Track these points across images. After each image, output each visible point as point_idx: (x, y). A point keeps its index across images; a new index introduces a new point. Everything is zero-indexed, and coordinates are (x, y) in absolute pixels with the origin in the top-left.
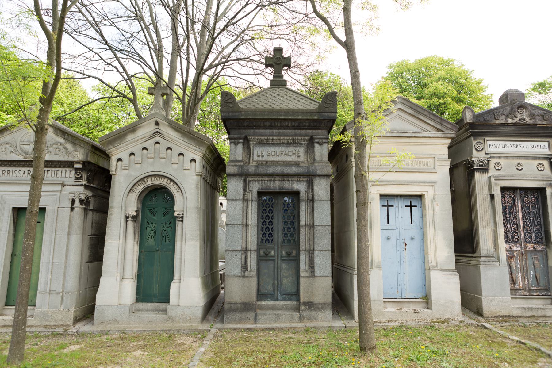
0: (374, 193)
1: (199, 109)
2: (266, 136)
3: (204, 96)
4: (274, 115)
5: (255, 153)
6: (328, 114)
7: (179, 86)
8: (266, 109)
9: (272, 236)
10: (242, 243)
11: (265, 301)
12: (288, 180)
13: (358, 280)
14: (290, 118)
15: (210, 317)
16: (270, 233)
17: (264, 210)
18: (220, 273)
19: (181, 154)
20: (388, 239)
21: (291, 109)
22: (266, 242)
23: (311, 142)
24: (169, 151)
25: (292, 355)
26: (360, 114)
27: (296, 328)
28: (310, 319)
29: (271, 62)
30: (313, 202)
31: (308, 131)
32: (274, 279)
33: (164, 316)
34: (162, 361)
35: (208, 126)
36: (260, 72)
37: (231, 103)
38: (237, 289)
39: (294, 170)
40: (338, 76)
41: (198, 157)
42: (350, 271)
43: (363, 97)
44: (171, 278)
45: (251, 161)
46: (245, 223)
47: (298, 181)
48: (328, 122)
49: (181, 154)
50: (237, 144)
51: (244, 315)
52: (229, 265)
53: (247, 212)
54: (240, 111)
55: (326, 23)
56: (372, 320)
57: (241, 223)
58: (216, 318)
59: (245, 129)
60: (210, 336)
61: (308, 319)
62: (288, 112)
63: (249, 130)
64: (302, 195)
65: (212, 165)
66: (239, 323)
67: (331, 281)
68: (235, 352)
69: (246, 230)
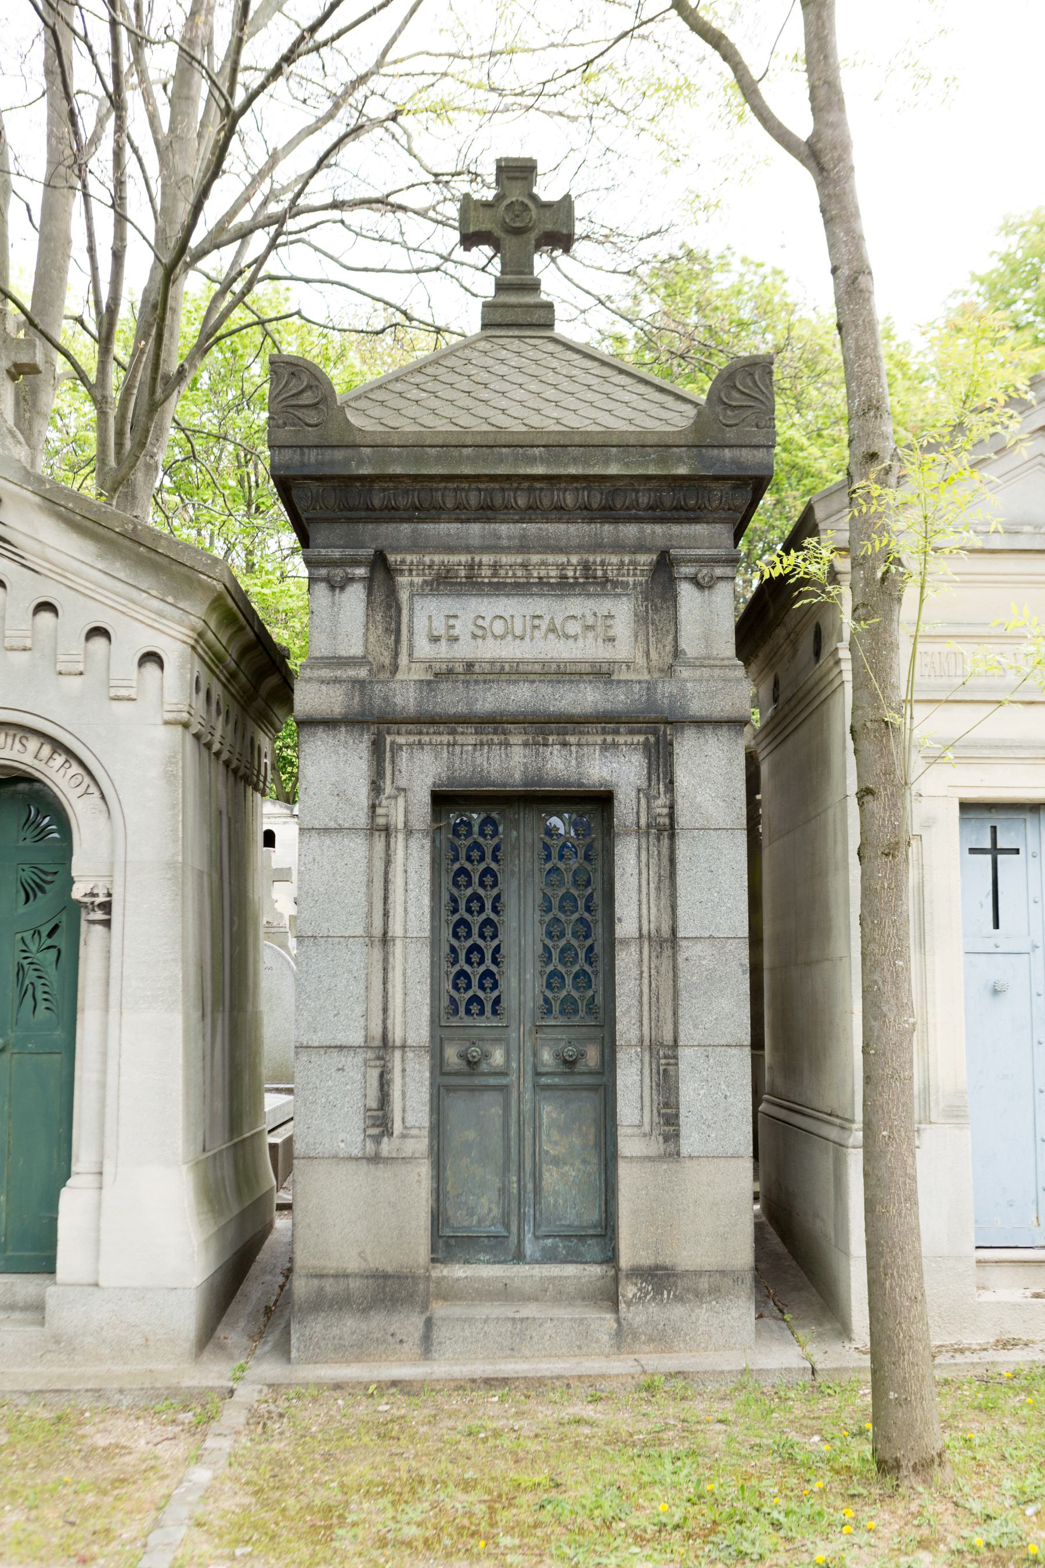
0: (932, 800)
1: (169, 423)
2: (468, 549)
3: (193, 366)
4: (501, 460)
5: (421, 624)
6: (736, 452)
7: (80, 320)
8: (466, 431)
9: (495, 986)
10: (366, 1015)
11: (467, 1262)
12: (565, 744)
13: (866, 1175)
14: (572, 471)
15: (232, 1335)
16: (488, 973)
17: (462, 871)
18: (271, 1139)
19: (98, 632)
20: (996, 992)
21: (574, 432)
22: (468, 1012)
23: (664, 572)
24: (46, 616)
25: (586, 1493)
26: (873, 457)
27: (603, 1376)
28: (662, 1339)
29: (484, 223)
30: (672, 837)
31: (648, 528)
32: (506, 1169)
33: (33, 1331)
34: (31, 1527)
35: (208, 495)
36: (436, 261)
37: (314, 406)
38: (347, 1211)
39: (588, 698)
40: (776, 272)
41: (174, 647)
42: (833, 1133)
43: (886, 365)
44: (61, 1171)
45: (403, 660)
46: (378, 931)
47: (605, 747)
48: (735, 488)
49: (98, 632)
50: (342, 588)
51: (377, 1321)
52: (311, 1108)
53: (386, 881)
54: (352, 443)
55: (725, 58)
56: (927, 1346)
57: (360, 931)
58: (258, 1335)
59: (377, 520)
60: (234, 1416)
61: (651, 1340)
62: (558, 445)
63: (391, 527)
64: (627, 808)
65: (233, 675)
66: (358, 1360)
67: (750, 1173)
68: (342, 1485)
69: (385, 960)
